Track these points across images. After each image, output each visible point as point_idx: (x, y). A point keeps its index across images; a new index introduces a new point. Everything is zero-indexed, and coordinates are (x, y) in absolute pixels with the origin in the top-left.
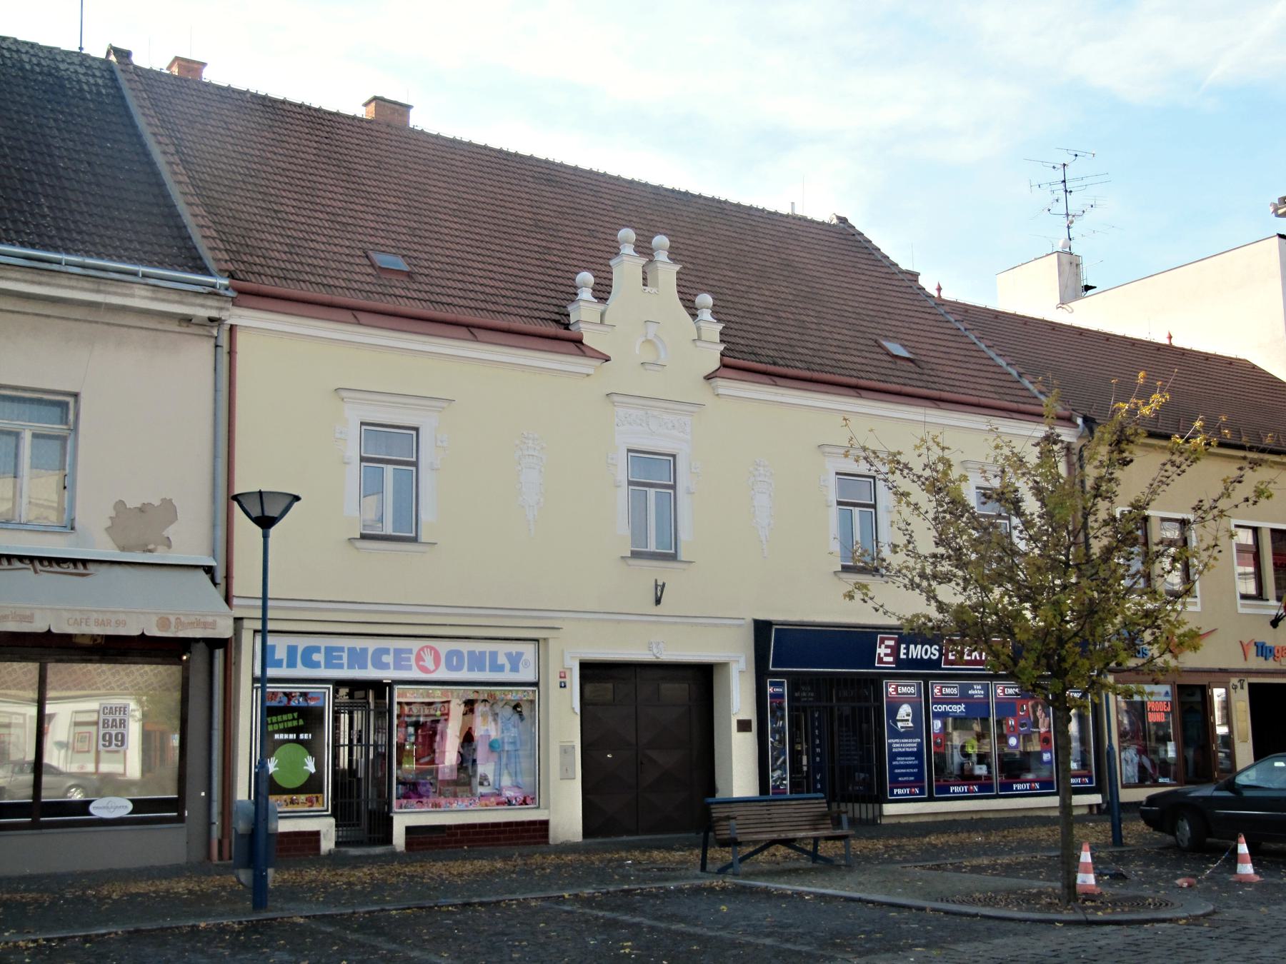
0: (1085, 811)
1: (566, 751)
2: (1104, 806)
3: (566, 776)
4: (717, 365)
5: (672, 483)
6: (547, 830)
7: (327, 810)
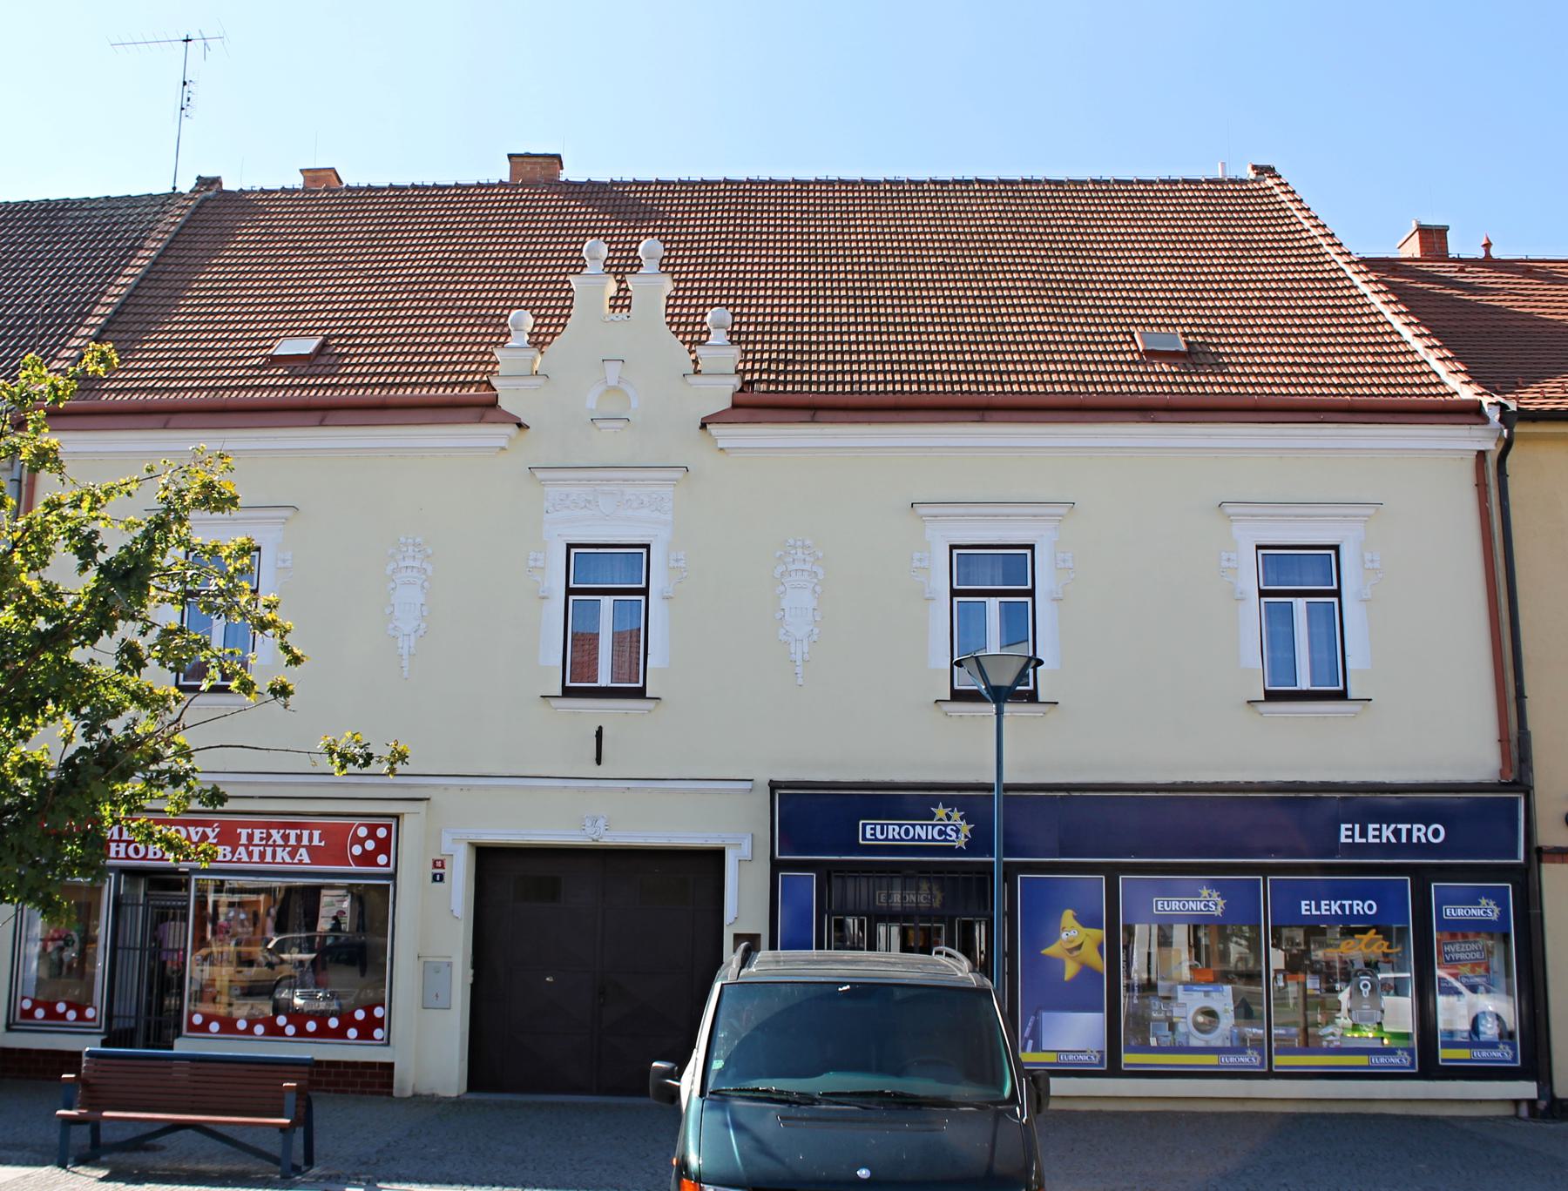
0: (1508, 1110)
1: (432, 970)
2: (1542, 1104)
3: (432, 1000)
4: (728, 404)
5: (1335, 587)
6: (391, 1076)
7: (100, 1027)
